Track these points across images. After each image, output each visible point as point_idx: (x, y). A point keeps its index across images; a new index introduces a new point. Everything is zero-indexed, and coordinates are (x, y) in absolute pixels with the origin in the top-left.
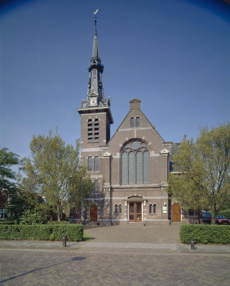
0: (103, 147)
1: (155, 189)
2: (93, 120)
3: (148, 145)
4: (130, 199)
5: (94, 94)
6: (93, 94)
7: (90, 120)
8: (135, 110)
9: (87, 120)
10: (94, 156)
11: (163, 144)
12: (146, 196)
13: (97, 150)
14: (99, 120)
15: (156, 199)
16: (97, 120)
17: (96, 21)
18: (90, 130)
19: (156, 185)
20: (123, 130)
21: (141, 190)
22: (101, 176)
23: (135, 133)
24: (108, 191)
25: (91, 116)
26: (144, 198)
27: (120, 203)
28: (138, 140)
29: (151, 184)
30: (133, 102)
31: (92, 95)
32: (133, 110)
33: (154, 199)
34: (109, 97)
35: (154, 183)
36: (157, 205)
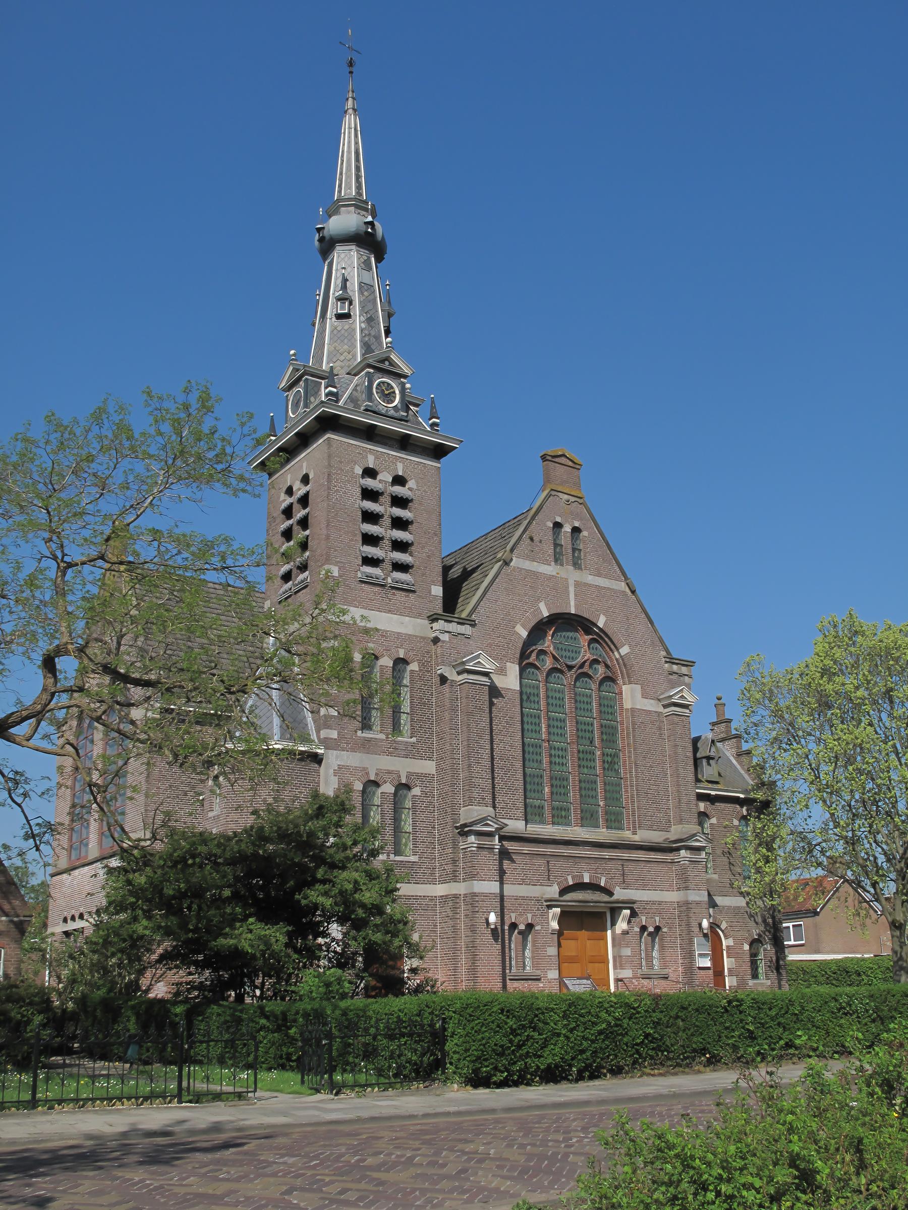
0: (463, 627)
1: (653, 856)
2: (386, 477)
3: (616, 653)
4: (568, 897)
5: (392, 363)
6: (388, 359)
7: (370, 473)
8: (566, 497)
9: (359, 471)
10: (389, 656)
11: (666, 662)
12: (625, 885)
13: (410, 631)
14: (866, 624)
15: (660, 903)
16: (399, 480)
17: (351, 64)
18: (370, 517)
19: (656, 837)
20: (527, 565)
21: (607, 854)
22: (429, 767)
23: (572, 589)
24: (492, 849)
25: (377, 458)
26: (620, 894)
27: (530, 916)
28: (577, 621)
29: (638, 832)
30: (556, 460)
31: (382, 361)
32: (561, 495)
33: (654, 903)
34: (292, 352)
35: (651, 828)
36: (665, 930)
